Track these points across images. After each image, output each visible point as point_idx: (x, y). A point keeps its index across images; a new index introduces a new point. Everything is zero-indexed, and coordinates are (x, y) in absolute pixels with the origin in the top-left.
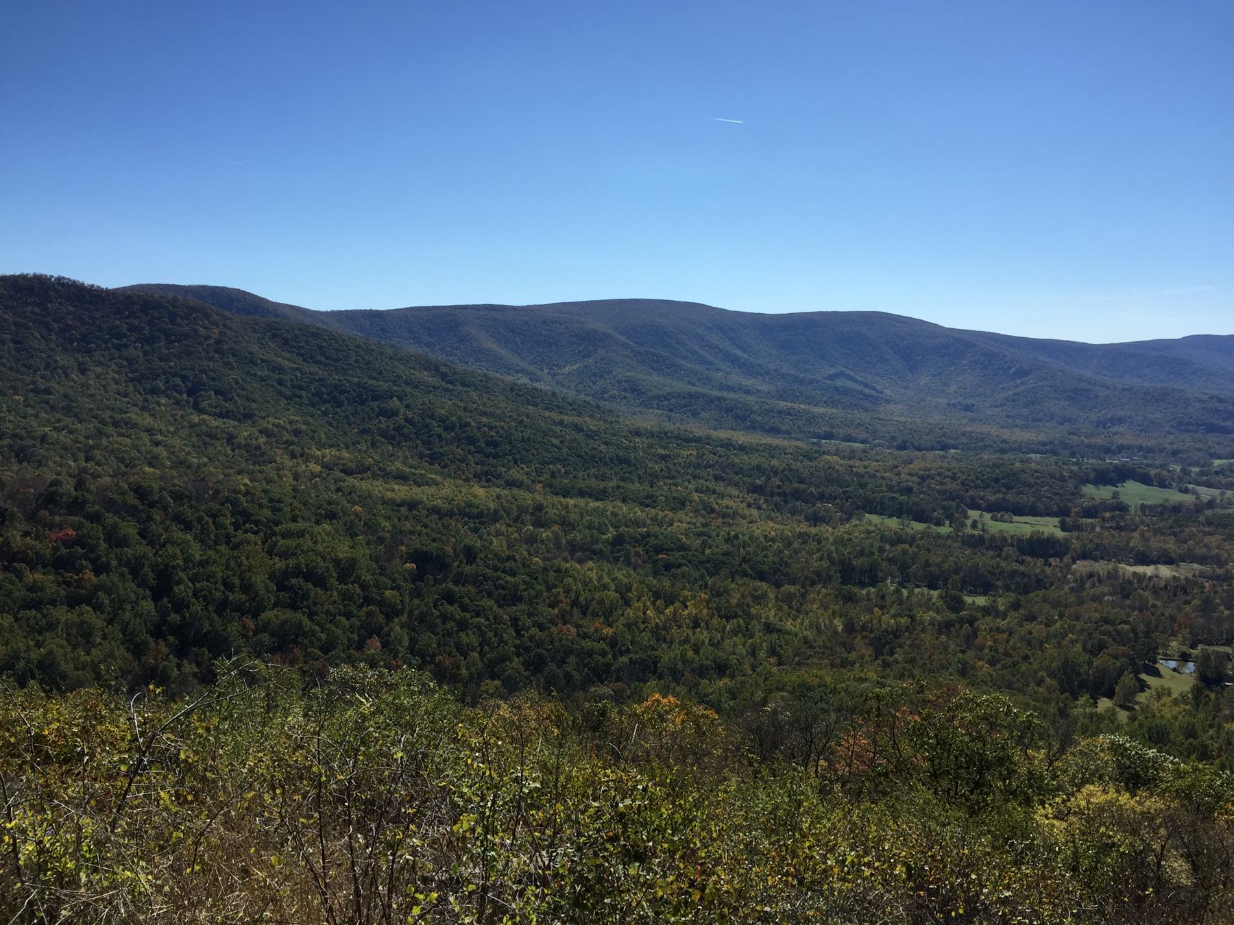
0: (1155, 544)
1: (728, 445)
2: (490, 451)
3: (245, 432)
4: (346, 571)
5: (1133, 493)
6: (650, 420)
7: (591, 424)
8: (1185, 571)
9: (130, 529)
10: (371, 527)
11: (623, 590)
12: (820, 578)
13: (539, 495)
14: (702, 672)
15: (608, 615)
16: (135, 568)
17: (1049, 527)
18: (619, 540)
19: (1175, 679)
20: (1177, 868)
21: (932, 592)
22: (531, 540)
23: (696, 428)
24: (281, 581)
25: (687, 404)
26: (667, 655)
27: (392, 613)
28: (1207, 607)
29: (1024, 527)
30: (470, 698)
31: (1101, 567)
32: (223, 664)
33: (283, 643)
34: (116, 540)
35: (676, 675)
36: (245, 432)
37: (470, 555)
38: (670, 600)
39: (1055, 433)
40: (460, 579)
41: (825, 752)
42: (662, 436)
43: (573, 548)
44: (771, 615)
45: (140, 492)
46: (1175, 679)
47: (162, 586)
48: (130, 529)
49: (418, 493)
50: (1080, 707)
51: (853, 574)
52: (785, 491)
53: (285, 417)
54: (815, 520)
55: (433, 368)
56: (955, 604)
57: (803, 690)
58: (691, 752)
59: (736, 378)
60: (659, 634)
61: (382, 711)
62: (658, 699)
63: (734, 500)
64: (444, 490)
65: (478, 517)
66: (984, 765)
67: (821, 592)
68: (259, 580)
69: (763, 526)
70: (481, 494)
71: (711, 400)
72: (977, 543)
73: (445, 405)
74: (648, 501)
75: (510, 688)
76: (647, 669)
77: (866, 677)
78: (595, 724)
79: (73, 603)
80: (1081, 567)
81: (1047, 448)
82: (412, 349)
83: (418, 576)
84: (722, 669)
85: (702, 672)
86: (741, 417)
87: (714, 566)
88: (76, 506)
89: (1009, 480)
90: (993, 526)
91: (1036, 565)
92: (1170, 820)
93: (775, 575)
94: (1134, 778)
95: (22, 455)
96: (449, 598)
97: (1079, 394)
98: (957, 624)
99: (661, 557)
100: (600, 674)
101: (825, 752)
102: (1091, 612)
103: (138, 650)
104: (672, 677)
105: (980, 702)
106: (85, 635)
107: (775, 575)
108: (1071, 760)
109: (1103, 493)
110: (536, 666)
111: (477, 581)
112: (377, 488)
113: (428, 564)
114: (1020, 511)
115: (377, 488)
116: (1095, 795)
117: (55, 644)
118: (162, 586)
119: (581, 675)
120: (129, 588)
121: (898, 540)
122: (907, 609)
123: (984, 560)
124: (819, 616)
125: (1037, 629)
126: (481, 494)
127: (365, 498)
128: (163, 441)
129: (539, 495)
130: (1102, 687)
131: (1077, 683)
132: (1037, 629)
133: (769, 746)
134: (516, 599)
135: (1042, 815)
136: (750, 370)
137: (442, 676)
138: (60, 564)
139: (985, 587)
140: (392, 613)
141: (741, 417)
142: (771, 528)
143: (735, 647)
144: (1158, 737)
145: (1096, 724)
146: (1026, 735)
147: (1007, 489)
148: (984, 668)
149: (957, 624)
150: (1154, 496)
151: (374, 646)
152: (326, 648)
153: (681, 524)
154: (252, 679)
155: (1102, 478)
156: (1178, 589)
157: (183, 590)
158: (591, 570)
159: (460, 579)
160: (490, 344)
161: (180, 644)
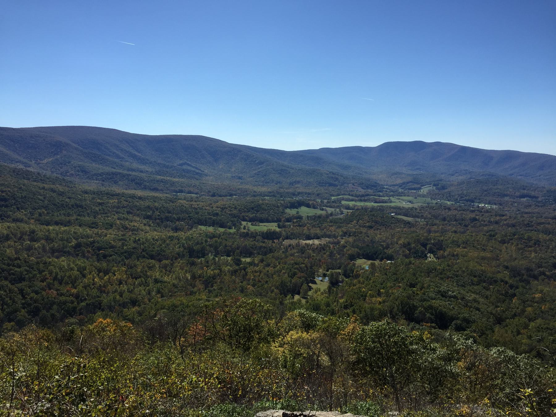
0: (313, 231)
1: (133, 197)
5: (304, 211)
6: (93, 186)
7: (61, 188)
8: (324, 241)
11: (81, 270)
12: (179, 256)
14: (124, 305)
17: (273, 227)
18: (78, 246)
19: (322, 284)
20: (325, 359)
22: (29, 249)
23: (116, 189)
25: (112, 178)
26: (105, 299)
28: (331, 255)
29: (264, 227)
31: (293, 242)
38: (106, 272)
41: (184, 334)
42: (99, 193)
43: (53, 251)
44: (157, 274)
46: (322, 284)
50: (288, 300)
51: (194, 253)
52: (162, 217)
54: (176, 230)
56: (238, 262)
59: (135, 165)
60: (102, 289)
62: (101, 320)
63: (137, 222)
67: (181, 262)
69: (152, 234)
72: (246, 235)
75: (20, 325)
76: (96, 307)
77: (202, 298)
80: (286, 242)
81: (272, 194)
84: (134, 303)
85: (124, 305)
86: (139, 183)
87: (129, 254)
89: (257, 208)
90: (253, 228)
91: (269, 243)
92: (321, 341)
93: (158, 256)
94: (308, 326)
97: (283, 172)
98: (239, 271)
99: (101, 252)
100: (71, 313)
101: (184, 334)
104: (108, 309)
107: (158, 256)
108: (285, 322)
110: (34, 312)
114: (262, 221)
116: (294, 335)
121: (213, 236)
123: (249, 242)
125: (270, 269)
130: (295, 291)
132: (270, 269)
133: (157, 335)
134: (21, 279)
135: (274, 347)
136: (143, 161)
141: (139, 183)
142: (156, 234)
143: (140, 292)
144: (316, 308)
145: (294, 306)
146: (267, 315)
147: (257, 213)
148: (250, 288)
149: (239, 271)
150: (311, 212)
153: (111, 236)
155: (293, 206)
156: (322, 248)
158: (63, 261)
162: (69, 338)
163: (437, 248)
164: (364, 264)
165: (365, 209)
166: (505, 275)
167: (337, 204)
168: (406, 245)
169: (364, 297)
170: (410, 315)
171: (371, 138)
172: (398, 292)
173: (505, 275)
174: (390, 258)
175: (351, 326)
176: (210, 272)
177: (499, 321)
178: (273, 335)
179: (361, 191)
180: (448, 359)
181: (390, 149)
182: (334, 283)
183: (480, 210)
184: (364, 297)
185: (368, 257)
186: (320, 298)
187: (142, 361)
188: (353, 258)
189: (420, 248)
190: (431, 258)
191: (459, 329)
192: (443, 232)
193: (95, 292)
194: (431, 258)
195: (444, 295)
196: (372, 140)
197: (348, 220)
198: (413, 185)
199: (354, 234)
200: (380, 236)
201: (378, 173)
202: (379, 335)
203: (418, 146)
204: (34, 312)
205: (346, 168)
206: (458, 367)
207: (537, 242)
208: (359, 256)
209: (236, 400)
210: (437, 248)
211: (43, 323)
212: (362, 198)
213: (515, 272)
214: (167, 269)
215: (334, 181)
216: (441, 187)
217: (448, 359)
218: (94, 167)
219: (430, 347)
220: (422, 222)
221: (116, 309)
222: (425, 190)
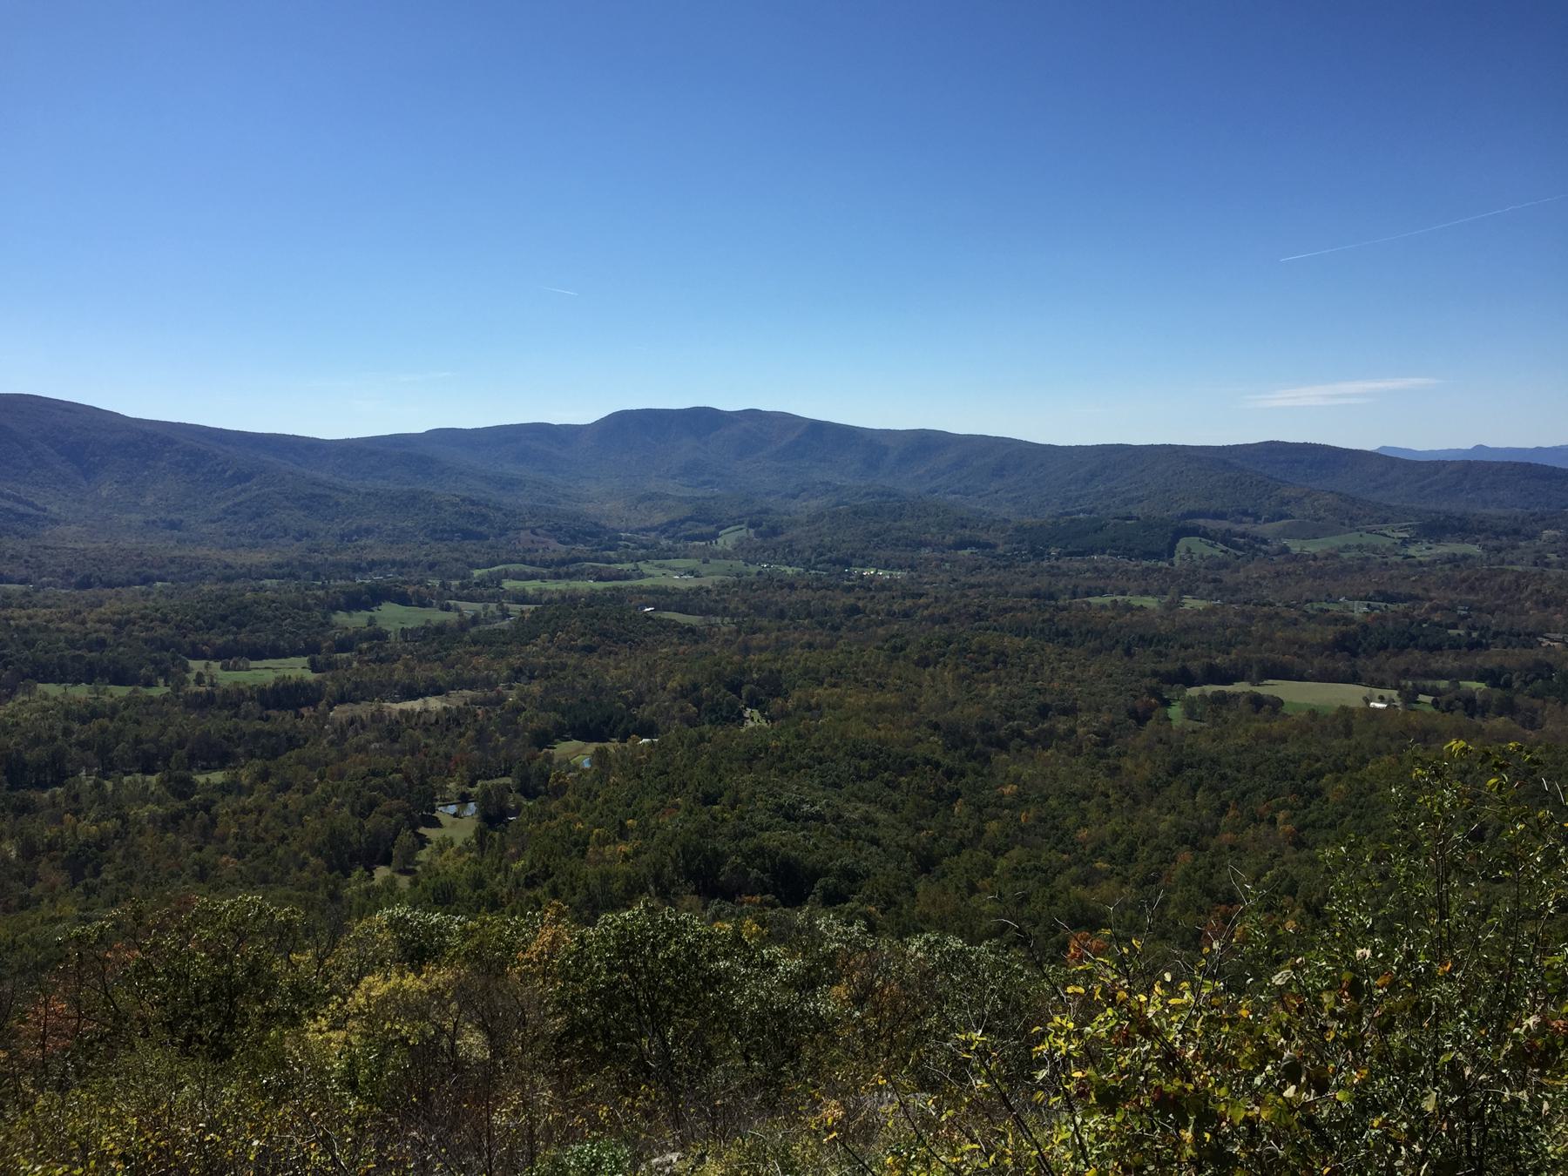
0: (422, 673)
5: (391, 616)
8: (457, 699)
17: (296, 669)
19: (456, 824)
20: (473, 1043)
28: (481, 738)
29: (265, 673)
31: (363, 710)
39: (293, 551)
46: (456, 824)
50: (353, 887)
56: (182, 788)
72: (204, 702)
77: (63, 918)
80: (340, 713)
81: (284, 571)
89: (239, 616)
90: (226, 678)
91: (284, 720)
94: (417, 953)
108: (346, 953)
109: (356, 621)
114: (257, 654)
116: (377, 985)
121: (91, 714)
123: (216, 724)
130: (377, 854)
132: (293, 799)
135: (315, 1031)
139: (222, 759)
144: (444, 898)
145: (374, 899)
146: (286, 938)
147: (237, 628)
148: (229, 863)
150: (414, 617)
155: (354, 602)
156: (451, 721)
163: (767, 692)
164: (577, 754)
165: (570, 600)
166: (933, 746)
168: (689, 692)
170: (708, 879)
173: (933, 746)
174: (648, 730)
175: (547, 934)
176: (88, 829)
177: (927, 864)
178: (307, 998)
179: (557, 549)
180: (807, 983)
182: (493, 818)
183: (867, 585)
184: (581, 846)
185: (586, 735)
186: (453, 866)
188: (544, 739)
189: (720, 698)
190: (754, 719)
191: (832, 899)
194: (754, 719)
195: (790, 814)
197: (525, 633)
198: (698, 526)
199: (546, 672)
200: (617, 671)
201: (601, 498)
202: (627, 946)
203: (702, 420)
205: (510, 484)
206: (831, 1000)
207: (1001, 658)
208: (562, 734)
210: (767, 692)
212: (561, 568)
213: (955, 737)
216: (767, 529)
217: (807, 983)
220: (725, 625)
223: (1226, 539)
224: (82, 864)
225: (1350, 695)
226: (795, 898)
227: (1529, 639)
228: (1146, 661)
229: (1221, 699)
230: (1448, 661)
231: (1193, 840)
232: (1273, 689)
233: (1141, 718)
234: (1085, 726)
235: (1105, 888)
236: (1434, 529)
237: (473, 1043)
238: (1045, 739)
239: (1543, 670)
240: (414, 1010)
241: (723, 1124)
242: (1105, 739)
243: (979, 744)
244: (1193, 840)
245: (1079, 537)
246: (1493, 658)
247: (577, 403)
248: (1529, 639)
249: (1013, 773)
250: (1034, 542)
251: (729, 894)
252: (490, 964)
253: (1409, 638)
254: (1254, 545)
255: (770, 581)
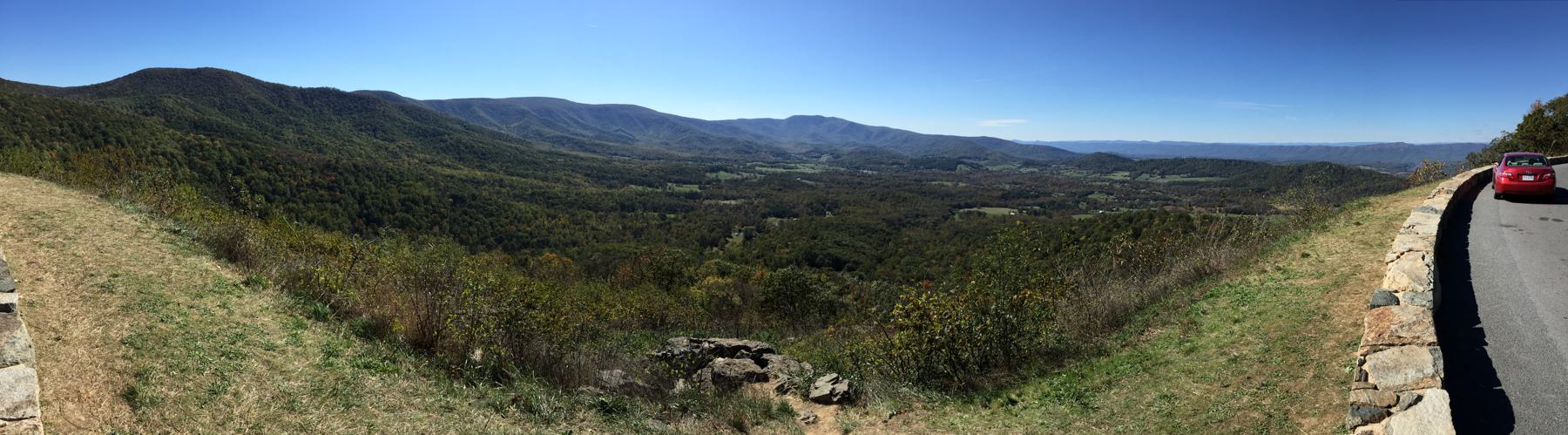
0: (730, 193)
1: (576, 157)
2: (481, 157)
3: (392, 146)
4: (427, 200)
5: (723, 175)
6: (546, 147)
7: (522, 148)
8: (739, 202)
9: (352, 179)
10: (436, 184)
11: (535, 213)
12: (613, 209)
13: (502, 175)
14: (566, 245)
15: (529, 223)
16: (353, 193)
17: (695, 188)
18: (533, 194)
19: (737, 238)
20: (737, 300)
21: (766, 385)
22: (498, 193)
23: (564, 150)
24: (403, 202)
25: (559, 141)
26: (552, 239)
27: (443, 217)
28: (746, 214)
29: (687, 188)
30: (473, 252)
31: (713, 202)
32: (382, 231)
33: (403, 225)
34: (348, 183)
35: (556, 246)
36: (392, 146)
37: (474, 197)
38: (554, 217)
39: (696, 153)
40: (470, 206)
41: (614, 274)
42: (550, 153)
43: (515, 196)
44: (594, 223)
45: (355, 166)
46: (737, 238)
47: (361, 200)
48: (352, 179)
49: (454, 172)
50: (707, 252)
51: (625, 207)
52: (598, 175)
53: (406, 141)
54: (611, 187)
55: (460, 123)
56: (663, 218)
57: (607, 252)
58: (562, 275)
59: (579, 131)
60: (550, 231)
61: (437, 252)
62: (548, 254)
63: (579, 179)
64: (464, 172)
65: (477, 183)
66: (673, 275)
67: (612, 215)
68: (395, 201)
69: (591, 189)
70: (479, 174)
71: (569, 139)
72: (671, 195)
73: (465, 138)
74: (545, 179)
75: (489, 248)
76: (544, 244)
77: (630, 246)
78: (523, 263)
79: (333, 202)
80: (706, 202)
81: (694, 159)
82: (453, 116)
83: (453, 204)
84: (574, 244)
85: (566, 245)
86: (582, 147)
87: (571, 205)
88: (335, 169)
89: (681, 171)
90: (677, 189)
91: (691, 202)
92: (735, 286)
93: (595, 208)
94: (723, 273)
95: (320, 150)
96: (465, 213)
97: (704, 139)
98: (665, 225)
99: (549, 200)
100: (526, 245)
101: (614, 274)
102: (710, 218)
103: (353, 222)
104: (554, 247)
105: (670, 252)
106: (335, 214)
107: (595, 208)
108: (703, 270)
109: (713, 175)
110: (500, 241)
111: (476, 207)
112: (439, 169)
113: (458, 200)
114: (686, 183)
115: (439, 169)
116: (711, 280)
117: (326, 215)
118: (361, 200)
119: (517, 244)
120: (351, 200)
121: (642, 195)
122: (646, 220)
123: (674, 201)
124: (613, 223)
125: (692, 225)
126: (479, 174)
127: (434, 174)
128: (363, 149)
129: (502, 175)
130: (714, 243)
131: (705, 243)
132: (692, 225)
133: (591, 271)
134: (492, 215)
135: (693, 289)
136: (584, 127)
137: (462, 242)
138: (330, 189)
139: (674, 212)
140: (443, 217)
141: (582, 147)
142: (594, 190)
143: (580, 235)
144: (732, 258)
145: (712, 256)
146: (688, 263)
147: (681, 175)
148: (674, 240)
149: (665, 225)
150: (729, 176)
151: (436, 229)
152: (419, 228)
153: (558, 188)
154: (392, 236)
155: (713, 170)
156: (738, 208)
157: (369, 201)
158: (522, 205)
159: (470, 206)
160: (482, 114)
161: (367, 221)
162: (524, 263)
163: (834, 206)
164: (774, 221)
165: (775, 174)
166: (883, 225)
167: (751, 169)
168: (810, 205)
169: (774, 248)
170: (812, 261)
171: (780, 111)
172: (802, 243)
173: (883, 225)
174: (796, 216)
175: (758, 271)
176: (639, 225)
177: (880, 260)
178: (692, 281)
179: (773, 159)
180: (841, 293)
181: (796, 121)
182: (748, 237)
183: (864, 175)
184: (774, 248)
185: (777, 216)
186: (736, 250)
187: (577, 290)
188: (764, 216)
189: (819, 208)
190: (829, 215)
191: (850, 270)
192: (839, 193)
193: (544, 232)
194: (829, 215)
195: (838, 244)
196: (782, 115)
197: (761, 183)
198: (815, 154)
199: (766, 196)
200: (788, 197)
201: (786, 143)
202: (785, 279)
203: (819, 120)
204: (500, 241)
205: (760, 137)
206: (848, 299)
207: (905, 199)
208: (770, 215)
209: (654, 327)
210: (834, 206)
211: (505, 249)
212: (773, 164)
213: (890, 223)
214: (602, 220)
215: (748, 149)
216: (836, 156)
217: (841, 293)
218: (547, 131)
219: (826, 286)
220: (822, 185)
221: (561, 247)
222: (824, 158)
223: (971, 165)
224: (637, 234)
225: (1005, 211)
226: (839, 269)
227: (1049, 194)
228: (947, 201)
229: (969, 213)
230: (1029, 201)
231: (961, 253)
232: (984, 210)
233: (946, 218)
234: (930, 221)
235: (935, 268)
236: (1028, 164)
237: (737, 300)
238: (917, 224)
239: (1053, 203)
240: (719, 288)
241: (808, 330)
242: (935, 224)
243: (897, 225)
244: (961, 253)
245: (929, 163)
246: (1041, 200)
247: (781, 113)
248: (1049, 194)
249: (908, 234)
250: (916, 164)
251: (819, 266)
252: (746, 278)
253: (1020, 195)
254: (978, 167)
255: (836, 172)
